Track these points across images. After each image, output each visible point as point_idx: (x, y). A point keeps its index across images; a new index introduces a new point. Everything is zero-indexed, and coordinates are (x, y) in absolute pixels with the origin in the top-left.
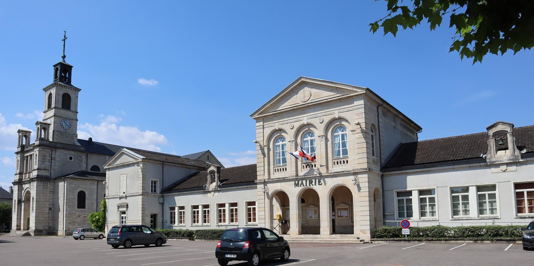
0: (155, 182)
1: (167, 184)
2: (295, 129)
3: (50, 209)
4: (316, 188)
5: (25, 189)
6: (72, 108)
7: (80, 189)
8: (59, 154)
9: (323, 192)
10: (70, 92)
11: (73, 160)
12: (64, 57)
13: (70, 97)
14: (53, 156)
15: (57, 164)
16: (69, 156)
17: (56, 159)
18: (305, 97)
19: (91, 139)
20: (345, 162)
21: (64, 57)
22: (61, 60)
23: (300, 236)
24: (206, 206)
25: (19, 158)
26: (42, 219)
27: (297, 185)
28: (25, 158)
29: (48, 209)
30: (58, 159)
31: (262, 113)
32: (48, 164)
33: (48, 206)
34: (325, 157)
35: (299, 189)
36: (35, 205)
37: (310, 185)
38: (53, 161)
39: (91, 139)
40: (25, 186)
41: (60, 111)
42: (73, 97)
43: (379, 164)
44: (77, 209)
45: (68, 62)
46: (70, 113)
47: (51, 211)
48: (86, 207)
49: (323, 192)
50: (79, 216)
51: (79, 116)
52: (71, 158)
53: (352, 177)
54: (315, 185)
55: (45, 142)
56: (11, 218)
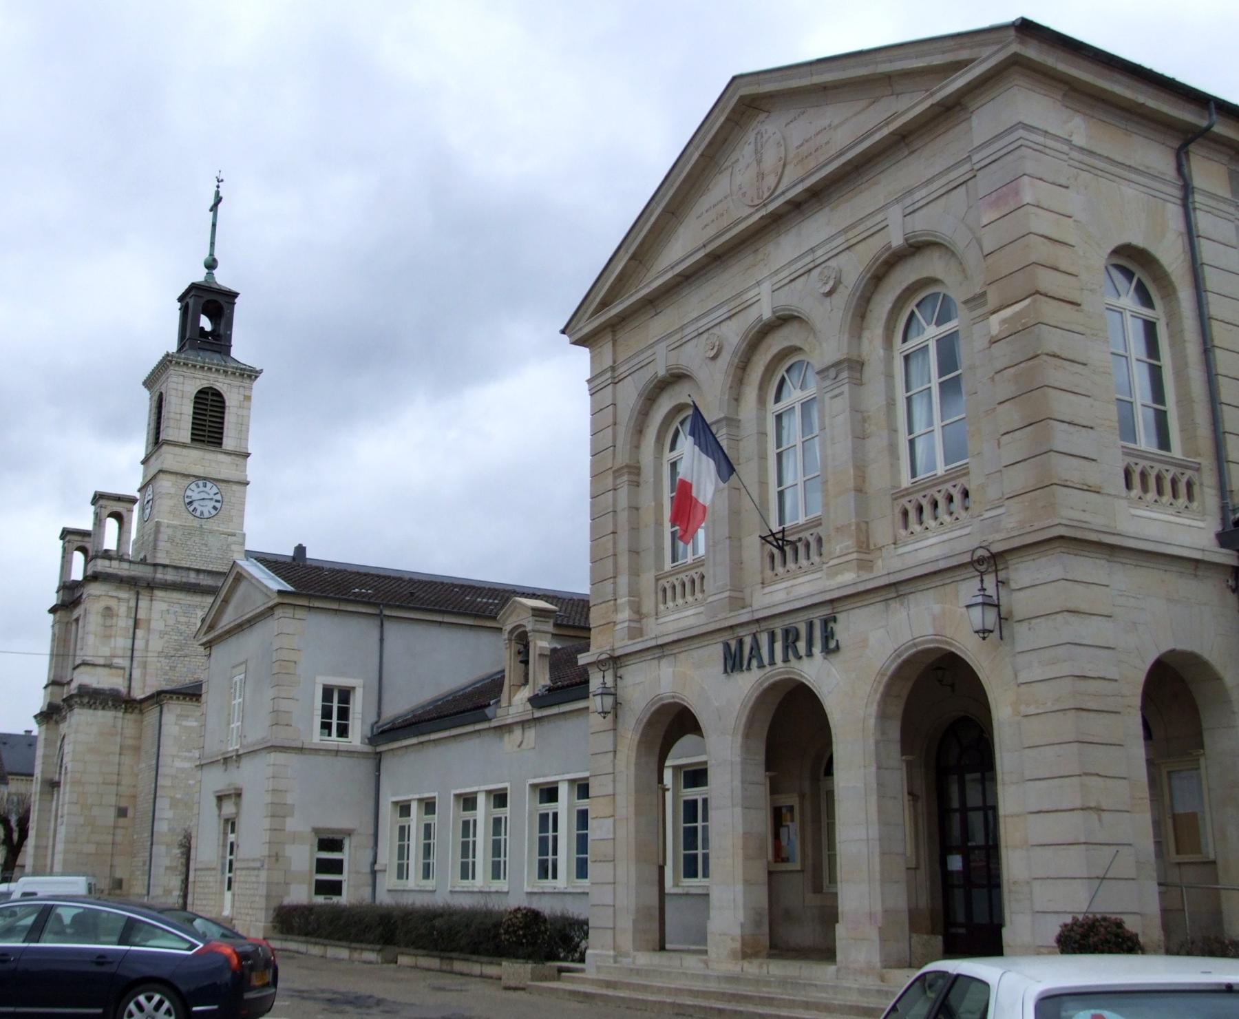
0: (345, 695)
1: (399, 705)
2: (726, 357)
3: (122, 812)
4: (814, 671)
6: (229, 442)
8: (164, 606)
9: (850, 689)
10: (221, 384)
12: (211, 265)
13: (223, 402)
14: (142, 615)
15: (156, 644)
17: (153, 625)
18: (761, 176)
19: (300, 550)
20: (957, 498)
21: (211, 265)
22: (200, 276)
23: (752, 968)
24: (500, 799)
26: (91, 848)
27: (734, 662)
29: (112, 812)
31: (604, 304)
32: (122, 643)
33: (113, 801)
35: (748, 683)
37: (786, 660)
38: (139, 633)
39: (300, 550)
41: (185, 451)
42: (232, 399)
43: (1209, 497)
45: (223, 278)
46: (222, 457)
47: (122, 821)
49: (850, 689)
51: (253, 469)
53: (969, 589)
54: (810, 654)
55: (115, 564)
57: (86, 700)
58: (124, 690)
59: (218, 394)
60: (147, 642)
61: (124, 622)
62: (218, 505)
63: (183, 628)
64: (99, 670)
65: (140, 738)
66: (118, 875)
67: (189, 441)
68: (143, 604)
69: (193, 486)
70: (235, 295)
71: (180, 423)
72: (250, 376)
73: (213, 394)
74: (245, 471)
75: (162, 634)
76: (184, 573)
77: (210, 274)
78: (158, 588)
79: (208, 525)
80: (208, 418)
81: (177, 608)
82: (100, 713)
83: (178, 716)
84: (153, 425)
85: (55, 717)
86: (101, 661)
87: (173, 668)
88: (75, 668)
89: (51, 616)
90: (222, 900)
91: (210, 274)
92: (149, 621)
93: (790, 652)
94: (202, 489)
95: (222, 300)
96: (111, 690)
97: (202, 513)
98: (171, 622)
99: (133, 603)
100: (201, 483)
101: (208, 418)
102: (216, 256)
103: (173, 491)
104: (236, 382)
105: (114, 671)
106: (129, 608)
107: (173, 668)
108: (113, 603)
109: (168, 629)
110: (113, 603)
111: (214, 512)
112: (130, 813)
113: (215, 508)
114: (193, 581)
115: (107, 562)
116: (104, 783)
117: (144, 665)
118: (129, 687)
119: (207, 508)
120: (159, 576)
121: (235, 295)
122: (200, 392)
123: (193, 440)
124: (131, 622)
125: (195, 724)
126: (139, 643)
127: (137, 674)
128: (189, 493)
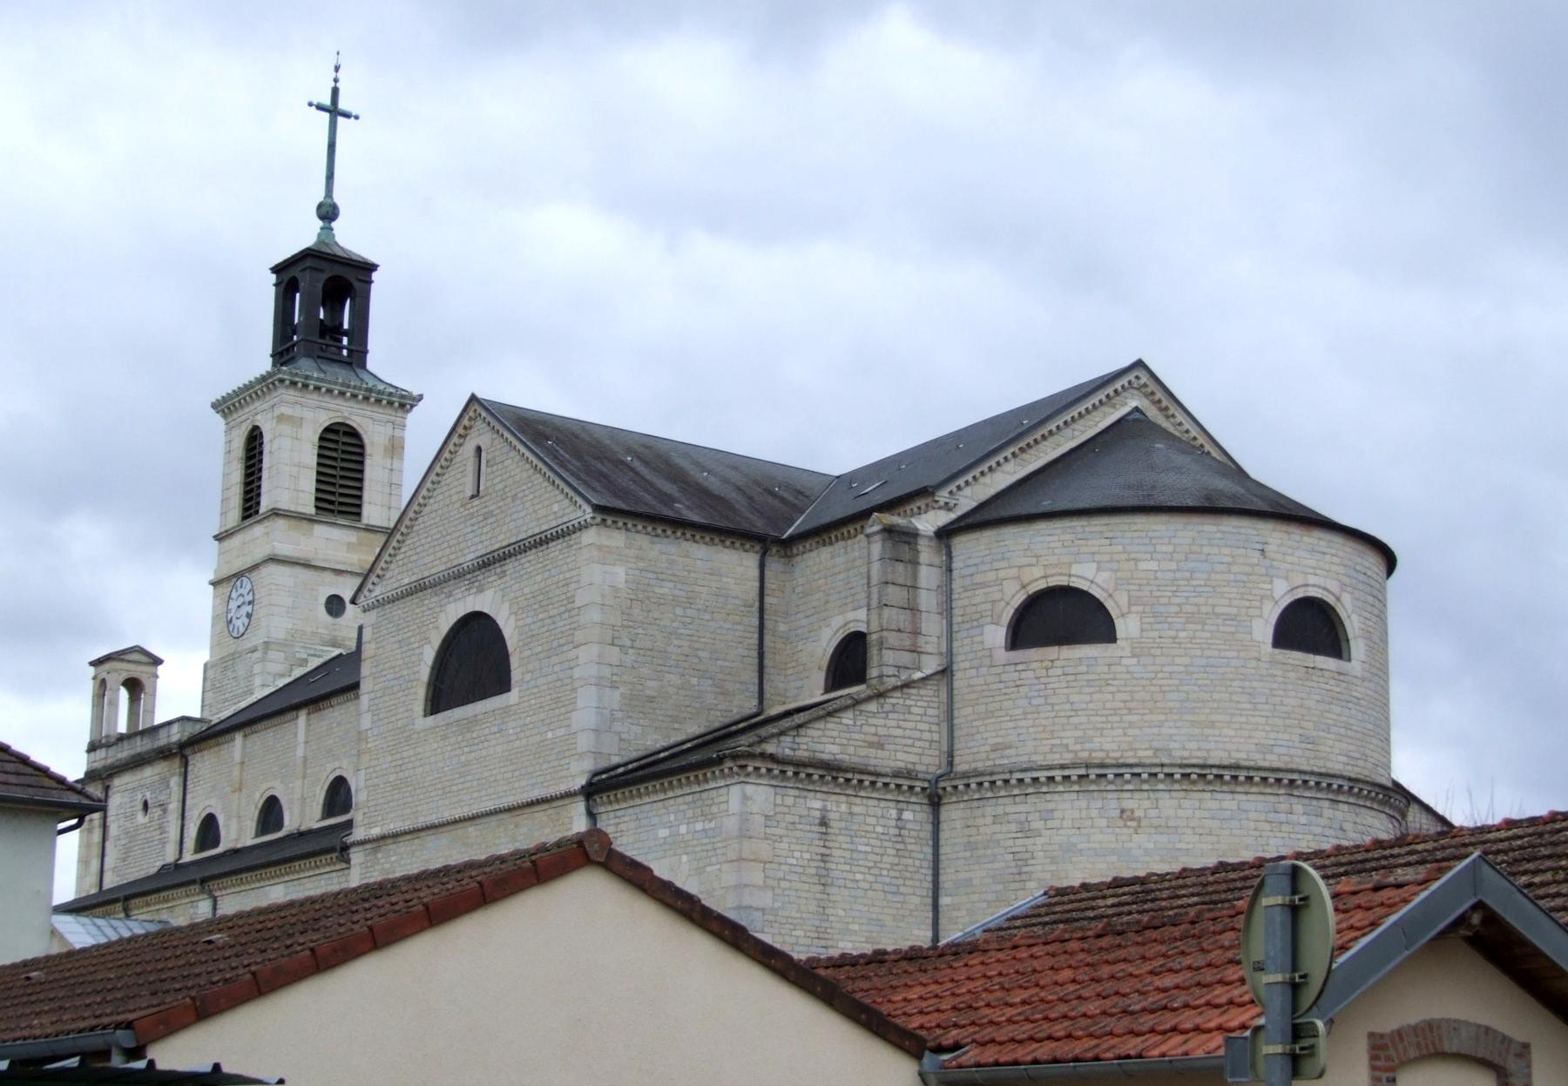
12: (328, 213)
13: (362, 446)
19: (217, 1067)
21: (328, 213)
22: (303, 234)
39: (217, 1067)
45: (351, 238)
59: (353, 433)
67: (312, 511)
70: (372, 267)
71: (292, 474)
72: (402, 406)
73: (345, 433)
77: (327, 229)
80: (340, 464)
84: (275, 721)
91: (327, 229)
93: (782, 747)
95: (350, 275)
101: (340, 464)
104: (382, 414)
121: (372, 267)
122: (327, 430)
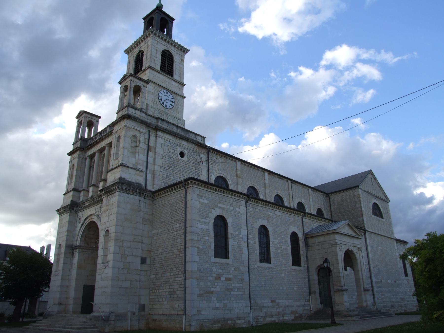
3: (144, 261)
5: (83, 219)
6: (176, 76)
7: (217, 212)
8: (162, 141)
10: (173, 51)
11: (185, 158)
14: (152, 144)
15: (159, 161)
16: (179, 150)
17: (158, 150)
25: (76, 162)
26: (127, 284)
28: (88, 160)
29: (139, 260)
30: (159, 151)
32: (142, 157)
34: (403, 270)
36: (111, 249)
38: (151, 154)
40: (84, 215)
42: (176, 58)
44: (213, 259)
47: (144, 267)
48: (230, 255)
50: (218, 278)
52: (182, 155)
55: (138, 112)
56: (55, 255)
57: (124, 187)
58: (143, 184)
60: (155, 159)
61: (143, 146)
62: (173, 104)
63: (172, 155)
64: (130, 170)
65: (152, 215)
66: (142, 302)
68: (152, 138)
69: (162, 92)
72: (184, 51)
74: (183, 92)
75: (162, 156)
76: (171, 126)
78: (160, 130)
79: (169, 112)
81: (168, 143)
82: (132, 196)
83: (198, 195)
85: (75, 209)
86: (131, 166)
87: (168, 177)
88: (108, 172)
89: (70, 157)
90: (182, 318)
92: (155, 148)
94: (166, 94)
96: (137, 183)
97: (166, 106)
98: (166, 151)
99: (147, 136)
100: (165, 91)
102: (162, 3)
103: (153, 91)
104: (179, 52)
105: (138, 172)
106: (145, 139)
107: (168, 177)
108: (137, 134)
109: (165, 154)
110: (137, 134)
111: (171, 107)
112: (148, 261)
113: (171, 105)
114: (175, 131)
115: (134, 111)
116: (134, 241)
117: (153, 173)
118: (146, 184)
119: (168, 104)
120: (160, 124)
123: (161, 69)
124: (146, 147)
125: (206, 202)
126: (151, 160)
127: (149, 176)
128: (160, 94)
